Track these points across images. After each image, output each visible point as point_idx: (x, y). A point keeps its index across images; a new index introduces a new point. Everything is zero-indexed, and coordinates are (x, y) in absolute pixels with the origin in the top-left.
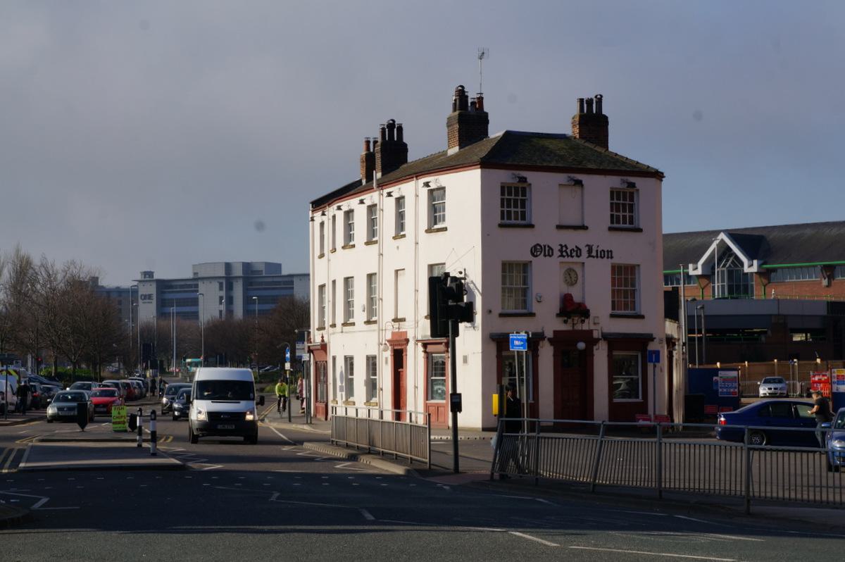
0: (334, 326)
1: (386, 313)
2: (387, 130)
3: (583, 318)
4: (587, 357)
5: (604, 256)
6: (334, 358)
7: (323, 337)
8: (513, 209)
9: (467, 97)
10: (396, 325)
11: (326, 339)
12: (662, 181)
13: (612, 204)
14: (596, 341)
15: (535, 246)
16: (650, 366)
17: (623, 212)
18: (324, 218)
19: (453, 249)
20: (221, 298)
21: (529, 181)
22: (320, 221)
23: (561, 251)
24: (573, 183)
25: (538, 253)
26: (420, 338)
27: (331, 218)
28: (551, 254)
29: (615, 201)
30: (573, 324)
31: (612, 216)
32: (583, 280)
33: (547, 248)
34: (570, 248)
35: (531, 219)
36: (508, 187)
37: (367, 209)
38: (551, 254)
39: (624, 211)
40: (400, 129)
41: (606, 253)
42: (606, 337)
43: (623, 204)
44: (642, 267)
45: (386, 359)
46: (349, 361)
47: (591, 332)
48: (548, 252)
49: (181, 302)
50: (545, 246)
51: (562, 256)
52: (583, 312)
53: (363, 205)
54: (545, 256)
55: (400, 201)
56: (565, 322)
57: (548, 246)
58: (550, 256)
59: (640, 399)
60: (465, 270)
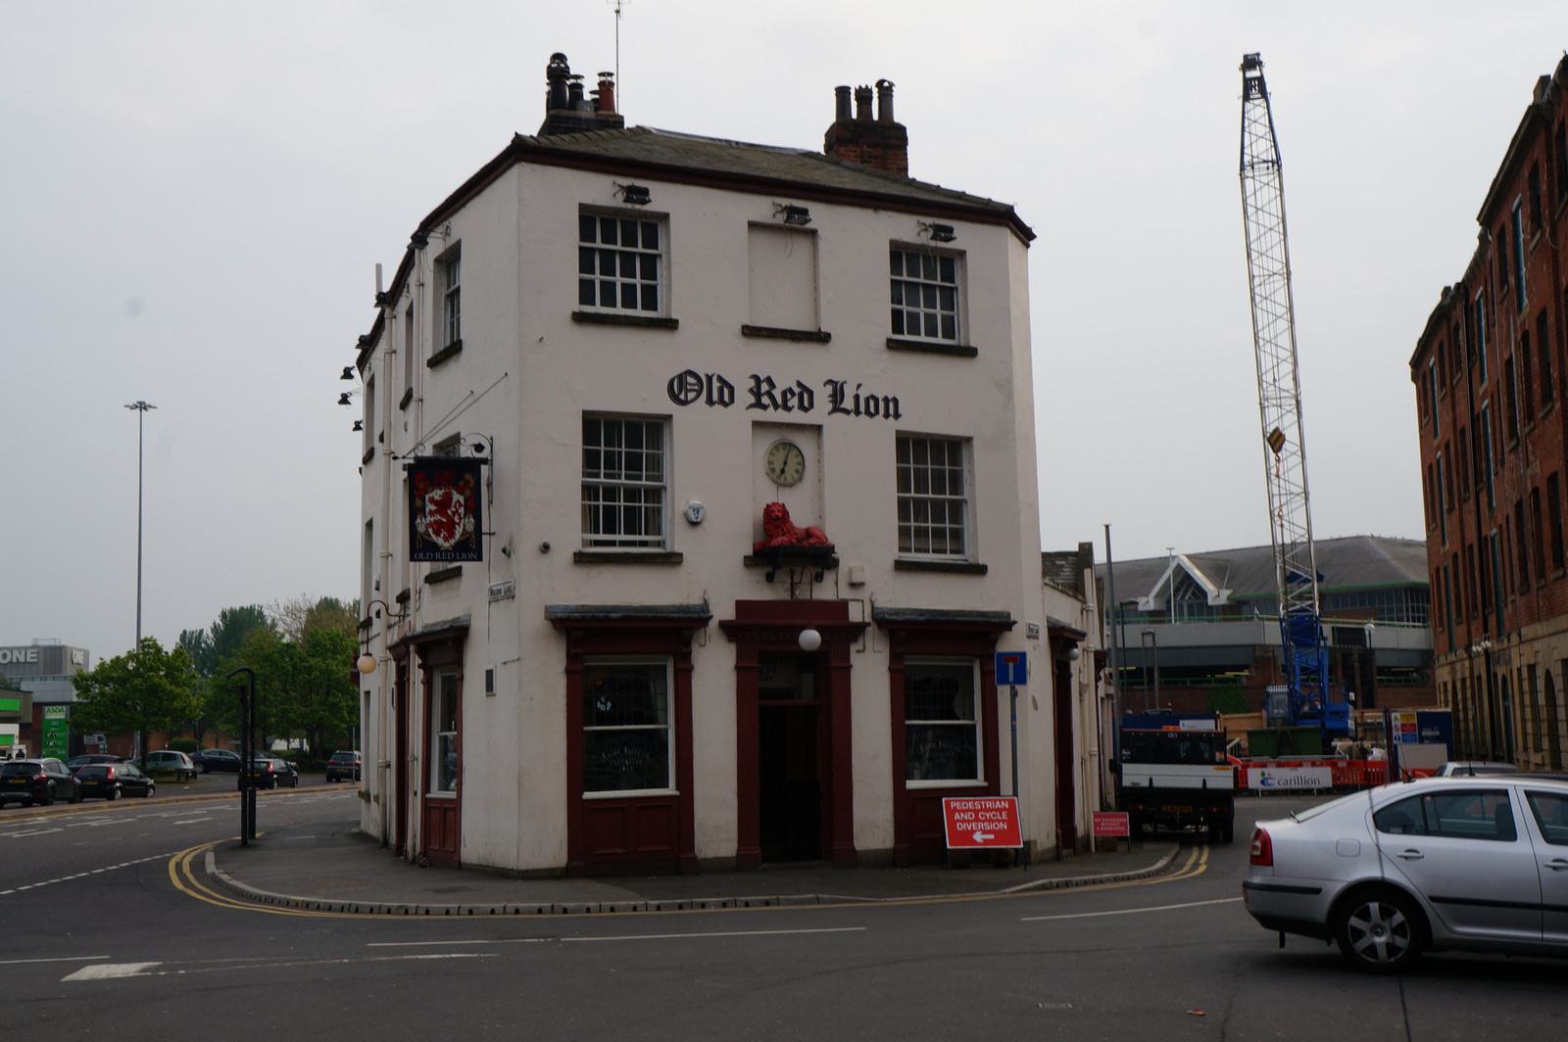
15: (681, 377)
23: (756, 393)
25: (691, 395)
33: (716, 385)
38: (726, 399)
51: (758, 404)
57: (720, 379)
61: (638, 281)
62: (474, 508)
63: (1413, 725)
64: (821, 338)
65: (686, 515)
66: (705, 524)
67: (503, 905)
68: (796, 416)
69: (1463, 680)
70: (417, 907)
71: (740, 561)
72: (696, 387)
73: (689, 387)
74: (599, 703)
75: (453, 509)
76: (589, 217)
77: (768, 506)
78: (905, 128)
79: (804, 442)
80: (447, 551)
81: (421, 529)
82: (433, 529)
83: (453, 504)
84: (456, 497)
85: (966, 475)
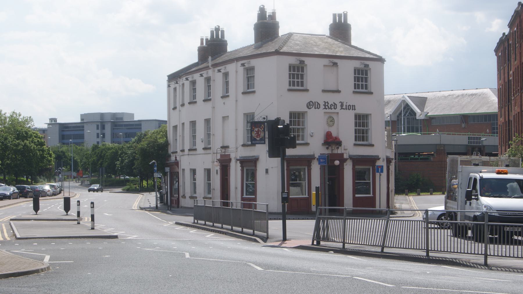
0: (183, 151)
1: (217, 144)
3: (338, 146)
4: (340, 168)
5: (350, 109)
6: (183, 170)
7: (176, 158)
8: (296, 80)
9: (266, 12)
10: (223, 151)
11: (178, 159)
12: (384, 63)
13: (290, 74)
14: (346, 160)
15: (309, 103)
16: (377, 175)
17: (361, 82)
18: (177, 85)
19: (272, 103)
20: (98, 134)
21: (306, 63)
22: (174, 87)
23: (325, 105)
24: (332, 64)
25: (311, 107)
26: (238, 158)
27: (181, 85)
28: (319, 107)
29: (357, 75)
30: (332, 150)
31: (355, 84)
33: (316, 104)
34: (330, 104)
37: (205, 80)
38: (319, 107)
39: (362, 81)
40: (223, 32)
41: (351, 107)
42: (351, 158)
43: (361, 77)
44: (372, 115)
45: (217, 171)
46: (194, 172)
47: (343, 154)
48: (317, 106)
49: (76, 137)
50: (315, 102)
51: (325, 108)
52: (338, 143)
53: (202, 77)
54: (315, 108)
55: (226, 75)
56: (327, 148)
57: (317, 103)
58: (318, 109)
60: (267, 117)
65: (310, 134)
71: (321, 144)
80: (258, 140)
81: (253, 135)
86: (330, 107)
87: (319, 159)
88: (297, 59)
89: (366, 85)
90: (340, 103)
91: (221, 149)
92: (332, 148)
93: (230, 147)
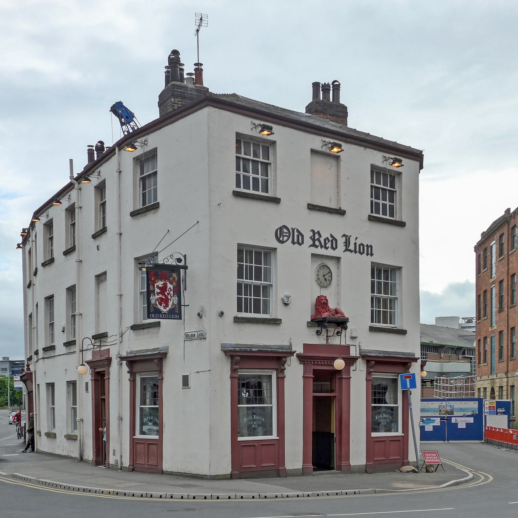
2: (95, 152)
15: (281, 228)
19: (198, 222)
23: (313, 239)
25: (285, 238)
26: (124, 354)
28: (300, 241)
30: (327, 336)
32: (339, 281)
33: (296, 234)
35: (275, 190)
36: (249, 285)
38: (300, 241)
45: (87, 384)
47: (348, 347)
51: (314, 245)
56: (318, 333)
58: (300, 244)
59: (274, 436)
60: (185, 256)
61: (259, 176)
62: (178, 291)
63: (494, 407)
64: (341, 212)
65: (282, 299)
66: (290, 305)
67: (146, 492)
68: (330, 252)
69: (501, 387)
70: (188, 495)
72: (287, 234)
73: (284, 234)
74: (243, 393)
75: (168, 292)
76: (240, 138)
77: (318, 296)
78: (347, 108)
79: (332, 265)
80: (165, 313)
81: (153, 302)
82: (159, 302)
83: (168, 289)
84: (169, 286)
85: (397, 287)
86: (323, 245)
87: (301, 358)
88: (254, 124)
89: (392, 208)
90: (344, 238)
91: (93, 340)
92: (327, 334)
93: (109, 335)
